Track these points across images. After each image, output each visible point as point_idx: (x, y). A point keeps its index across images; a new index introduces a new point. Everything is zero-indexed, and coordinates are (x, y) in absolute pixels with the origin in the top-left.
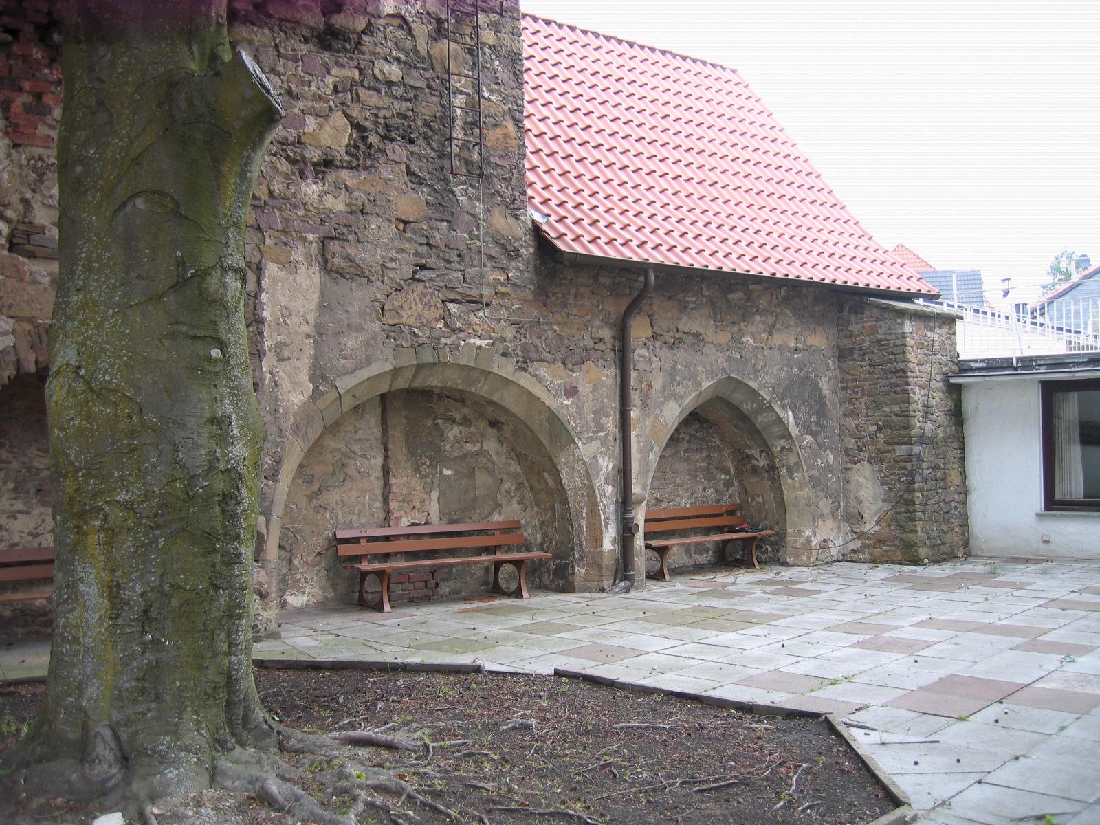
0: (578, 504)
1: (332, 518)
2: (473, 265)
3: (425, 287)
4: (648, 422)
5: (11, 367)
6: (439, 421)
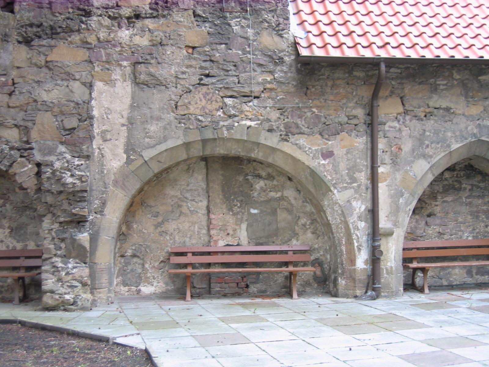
0: (340, 234)
1: (171, 239)
2: (245, 72)
3: (208, 89)
4: (398, 176)
6: (249, 177)
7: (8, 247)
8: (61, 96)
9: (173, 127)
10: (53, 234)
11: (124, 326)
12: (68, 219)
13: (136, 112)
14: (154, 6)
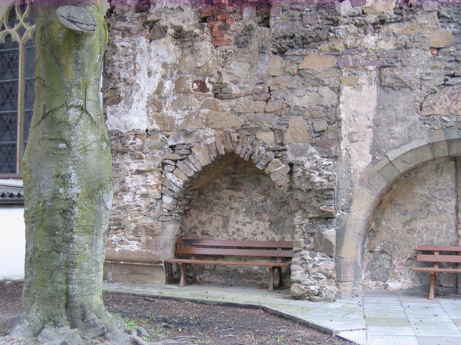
1: (419, 237)
5: (214, 153)
7: (268, 238)
8: (312, 101)
9: (418, 127)
10: (303, 228)
11: (357, 319)
12: (316, 215)
13: (381, 114)
14: (398, 11)
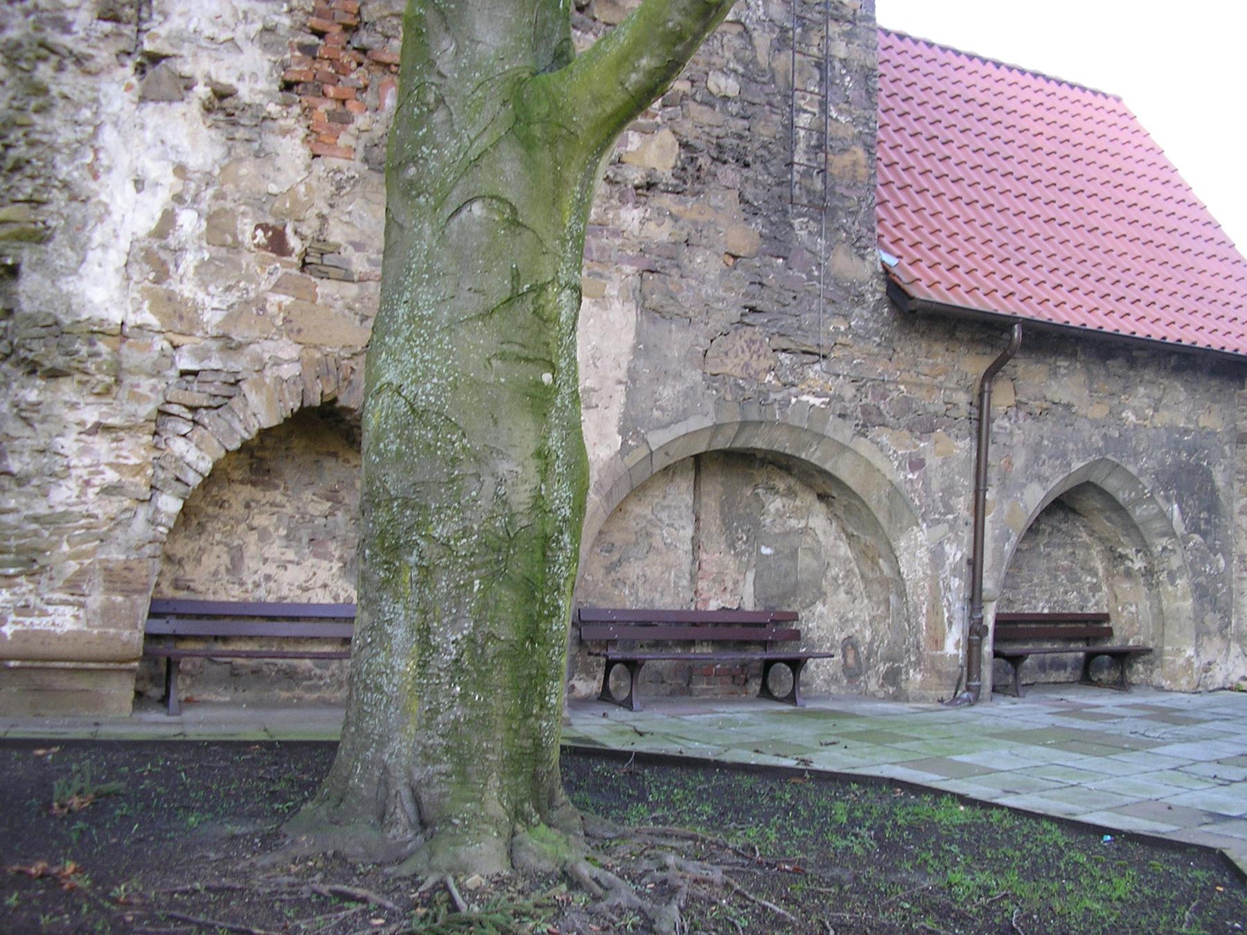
7: (336, 598)
